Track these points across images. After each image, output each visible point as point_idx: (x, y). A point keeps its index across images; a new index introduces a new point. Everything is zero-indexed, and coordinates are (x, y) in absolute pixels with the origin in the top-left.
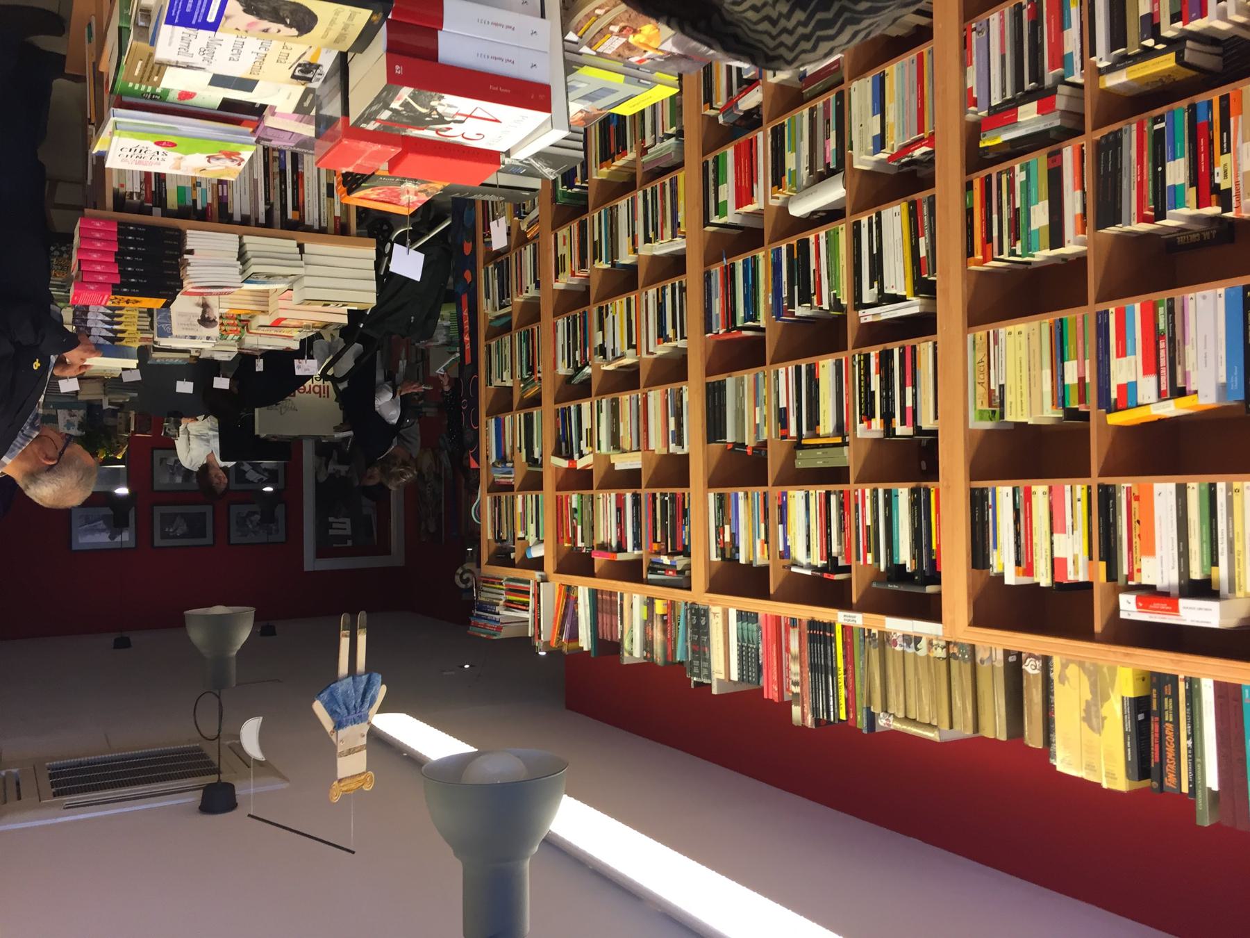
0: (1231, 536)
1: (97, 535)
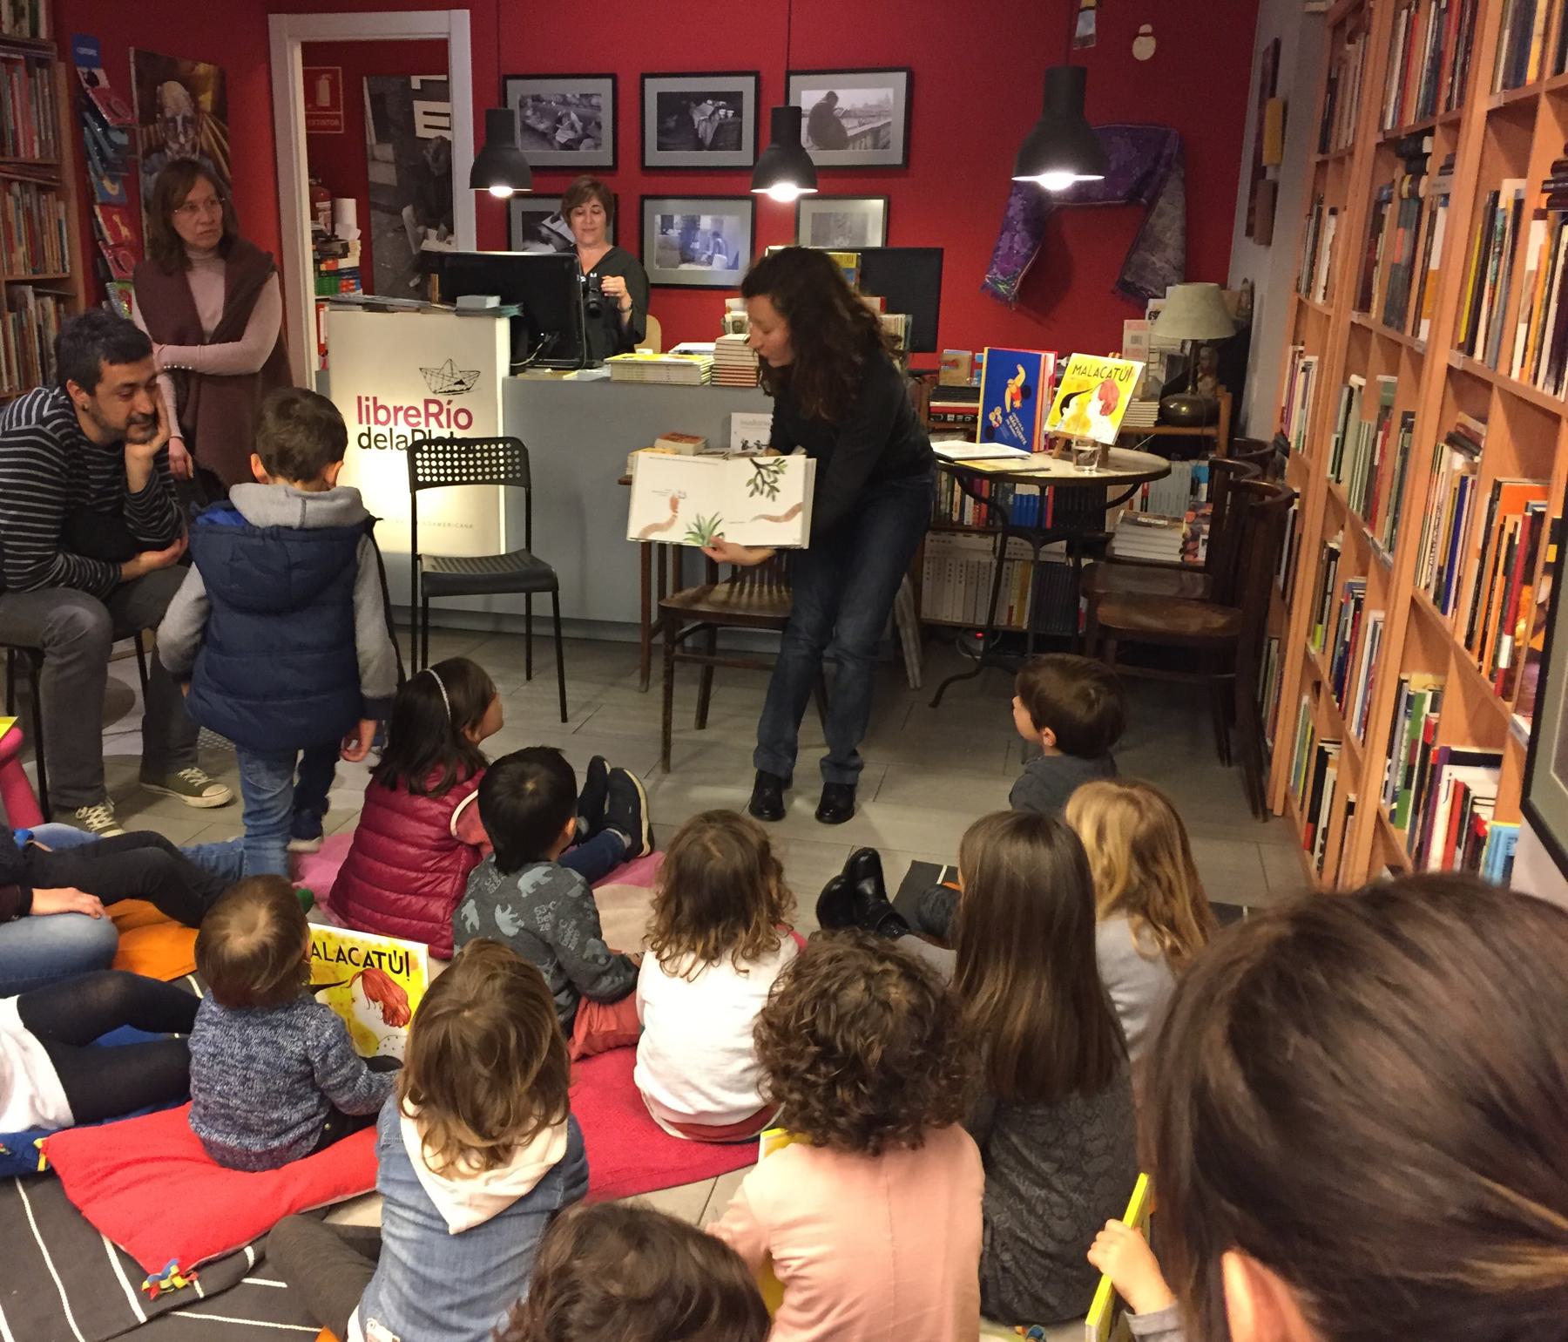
0: (1333, 75)
1: (859, 105)
